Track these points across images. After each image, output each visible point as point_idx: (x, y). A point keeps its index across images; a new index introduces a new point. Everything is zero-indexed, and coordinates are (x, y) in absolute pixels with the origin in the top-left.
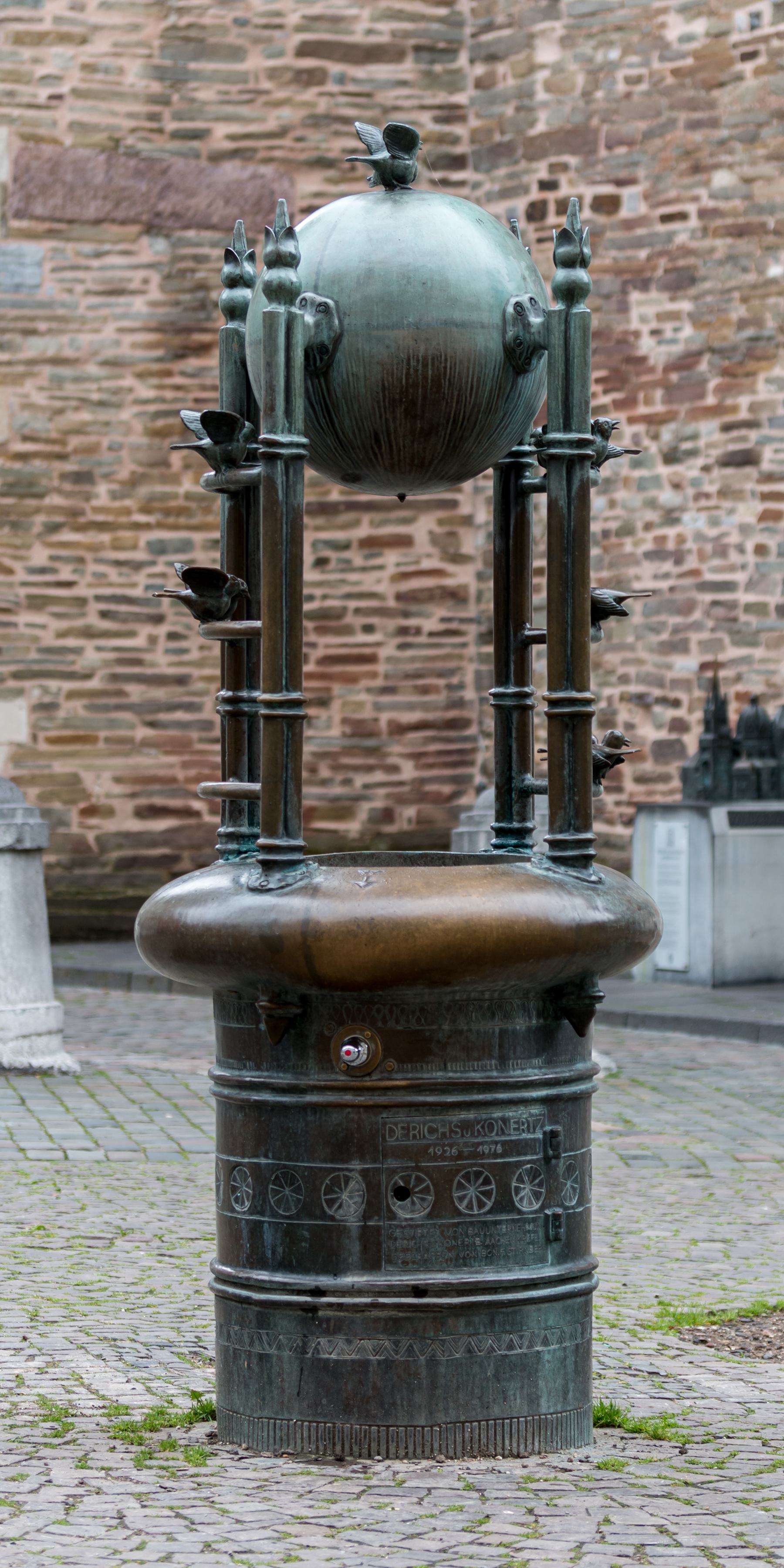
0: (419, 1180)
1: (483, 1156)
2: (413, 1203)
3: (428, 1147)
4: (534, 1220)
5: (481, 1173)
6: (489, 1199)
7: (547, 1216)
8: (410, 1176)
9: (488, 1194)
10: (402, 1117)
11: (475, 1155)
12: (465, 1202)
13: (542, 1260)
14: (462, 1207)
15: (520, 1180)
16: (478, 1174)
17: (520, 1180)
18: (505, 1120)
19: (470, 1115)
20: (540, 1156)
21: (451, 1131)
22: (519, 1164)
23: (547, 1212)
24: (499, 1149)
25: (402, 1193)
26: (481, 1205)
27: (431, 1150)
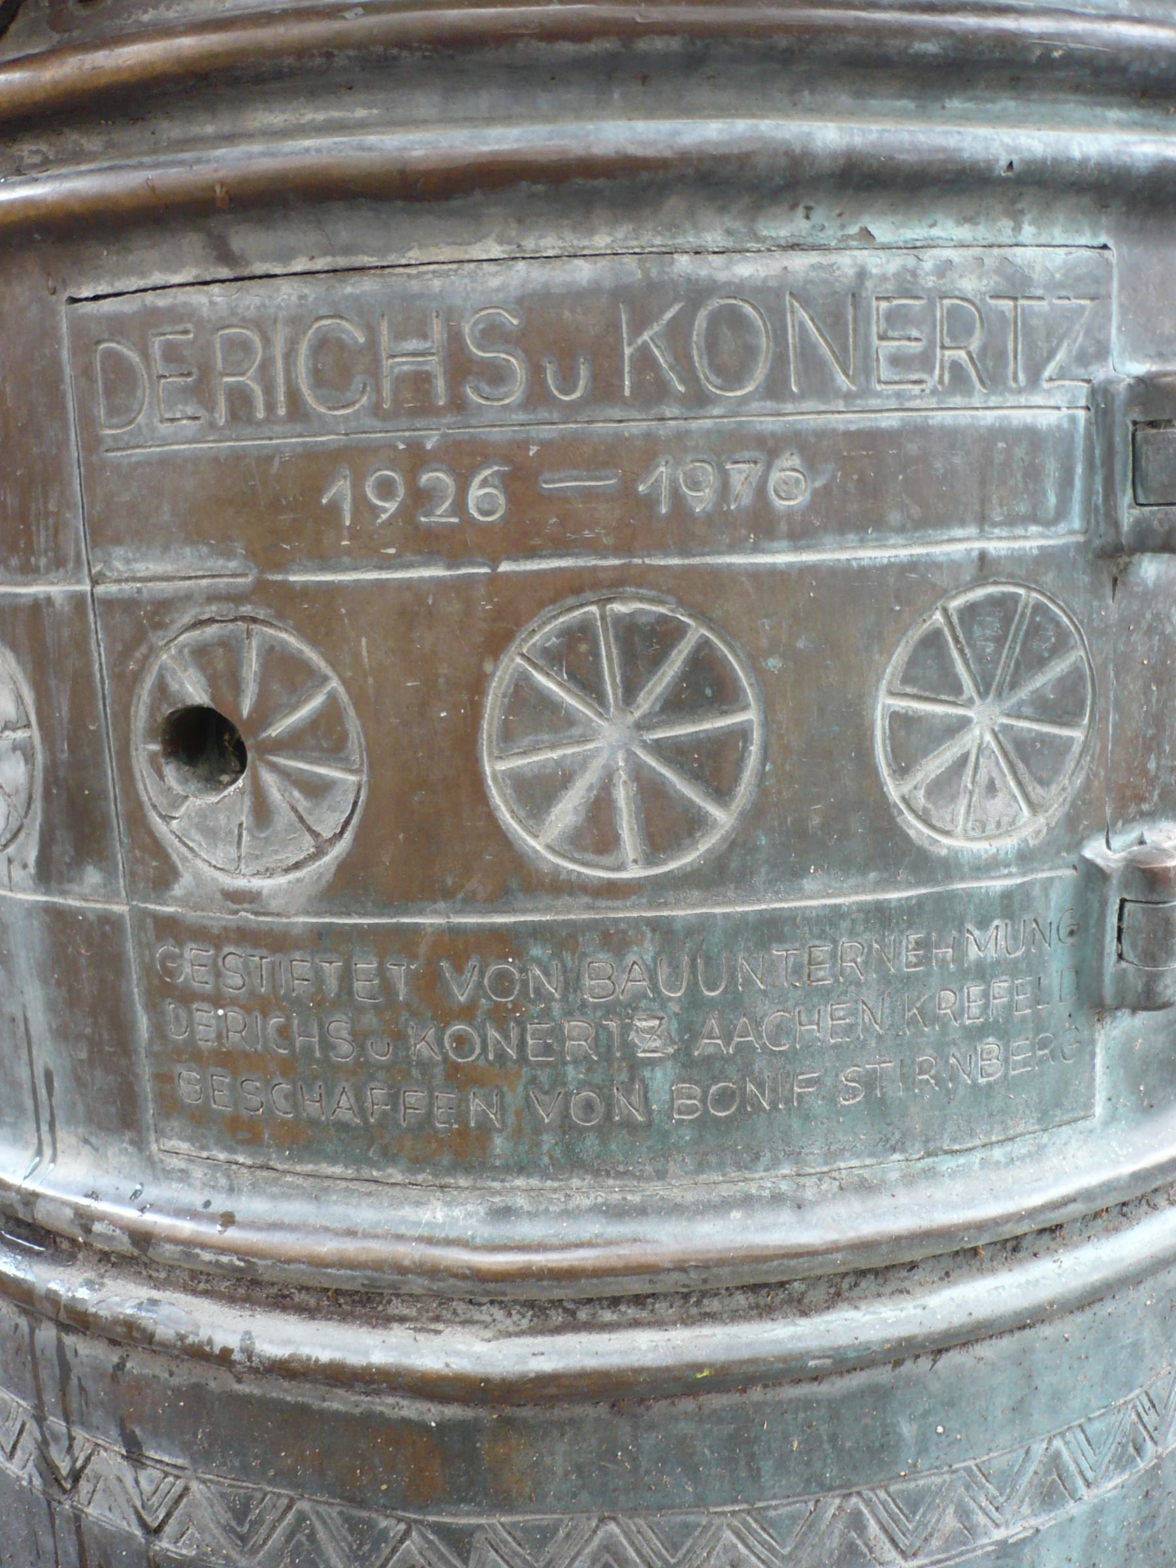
0: (288, 674)
1: (684, 530)
2: (262, 811)
3: (318, 466)
4: (1009, 905)
5: (664, 635)
6: (721, 793)
7: (1093, 875)
8: (231, 648)
9: (712, 764)
10: (168, 283)
11: (638, 524)
12: (566, 812)
13: (1058, 1106)
14: (541, 842)
15: (930, 671)
16: (644, 644)
17: (930, 671)
18: (841, 309)
19: (582, 260)
20: (1066, 534)
21: (460, 366)
22: (912, 585)
23: (1095, 850)
24: (791, 486)
25: (205, 741)
26: (667, 826)
27: (340, 490)
